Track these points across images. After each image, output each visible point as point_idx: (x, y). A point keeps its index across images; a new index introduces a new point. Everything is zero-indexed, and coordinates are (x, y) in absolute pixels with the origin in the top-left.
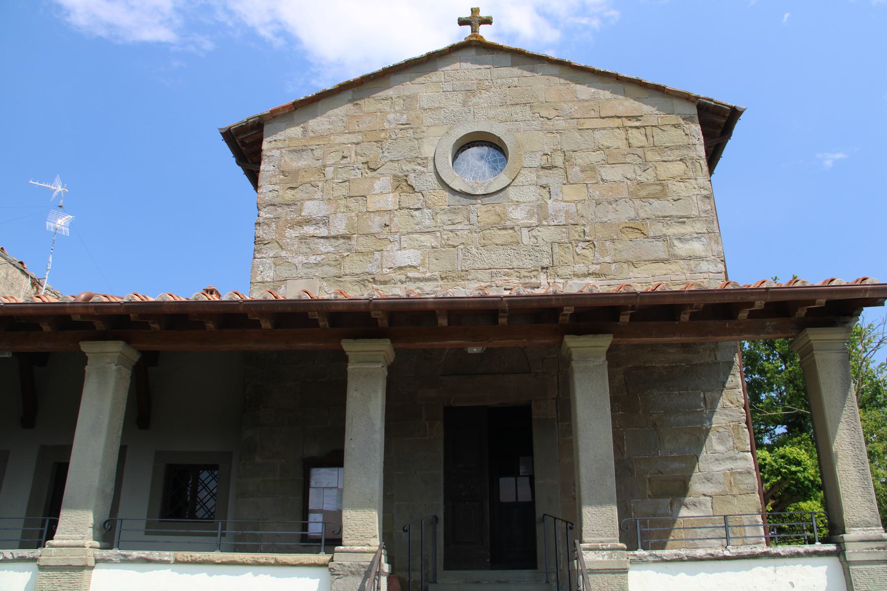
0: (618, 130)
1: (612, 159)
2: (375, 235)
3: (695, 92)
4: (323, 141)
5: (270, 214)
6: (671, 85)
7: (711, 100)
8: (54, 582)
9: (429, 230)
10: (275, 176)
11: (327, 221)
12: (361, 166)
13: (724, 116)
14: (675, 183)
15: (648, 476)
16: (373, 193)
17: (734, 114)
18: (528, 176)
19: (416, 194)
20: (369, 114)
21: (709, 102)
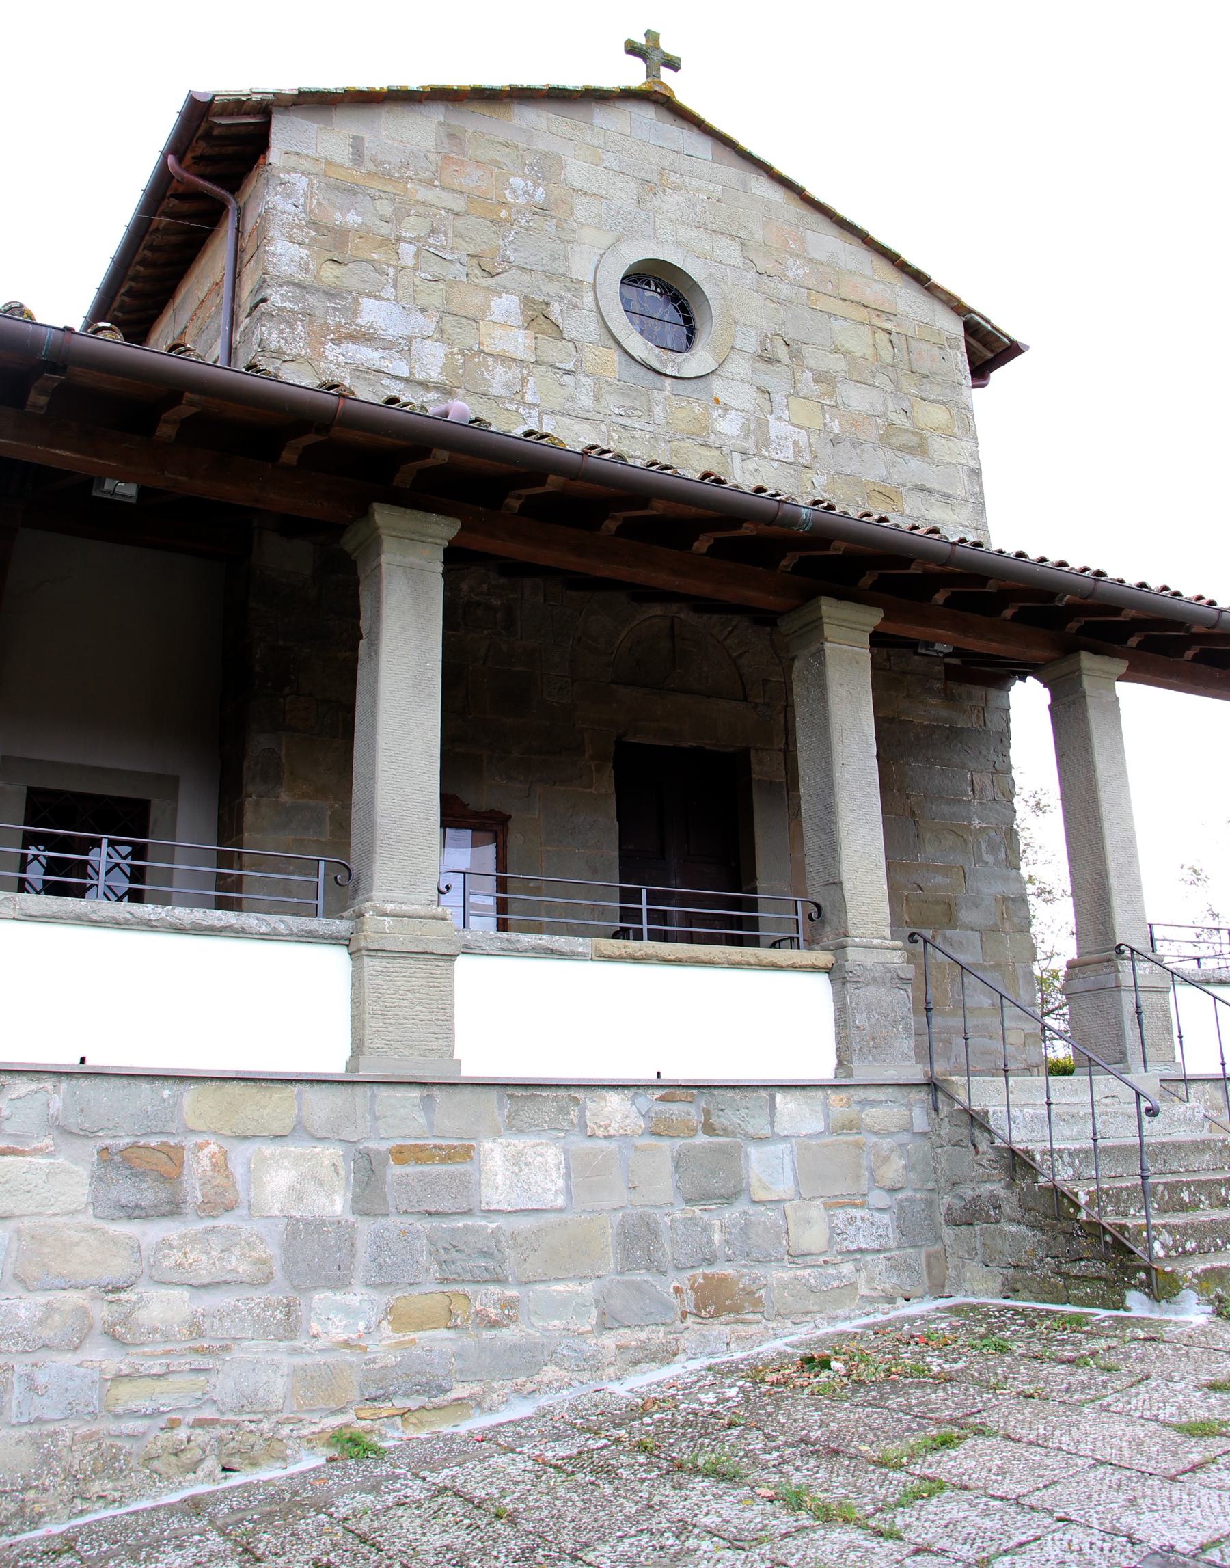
0: (861, 327)
1: (857, 374)
2: (497, 399)
3: (968, 301)
4: (393, 187)
5: (290, 301)
6: (937, 278)
7: (988, 321)
8: (399, 984)
9: (588, 415)
10: (300, 228)
11: (407, 348)
12: (465, 259)
13: (992, 351)
14: (935, 437)
15: (906, 893)
16: (491, 318)
17: (1012, 350)
18: (739, 367)
19: (564, 341)
20: (478, 163)
21: (984, 323)
